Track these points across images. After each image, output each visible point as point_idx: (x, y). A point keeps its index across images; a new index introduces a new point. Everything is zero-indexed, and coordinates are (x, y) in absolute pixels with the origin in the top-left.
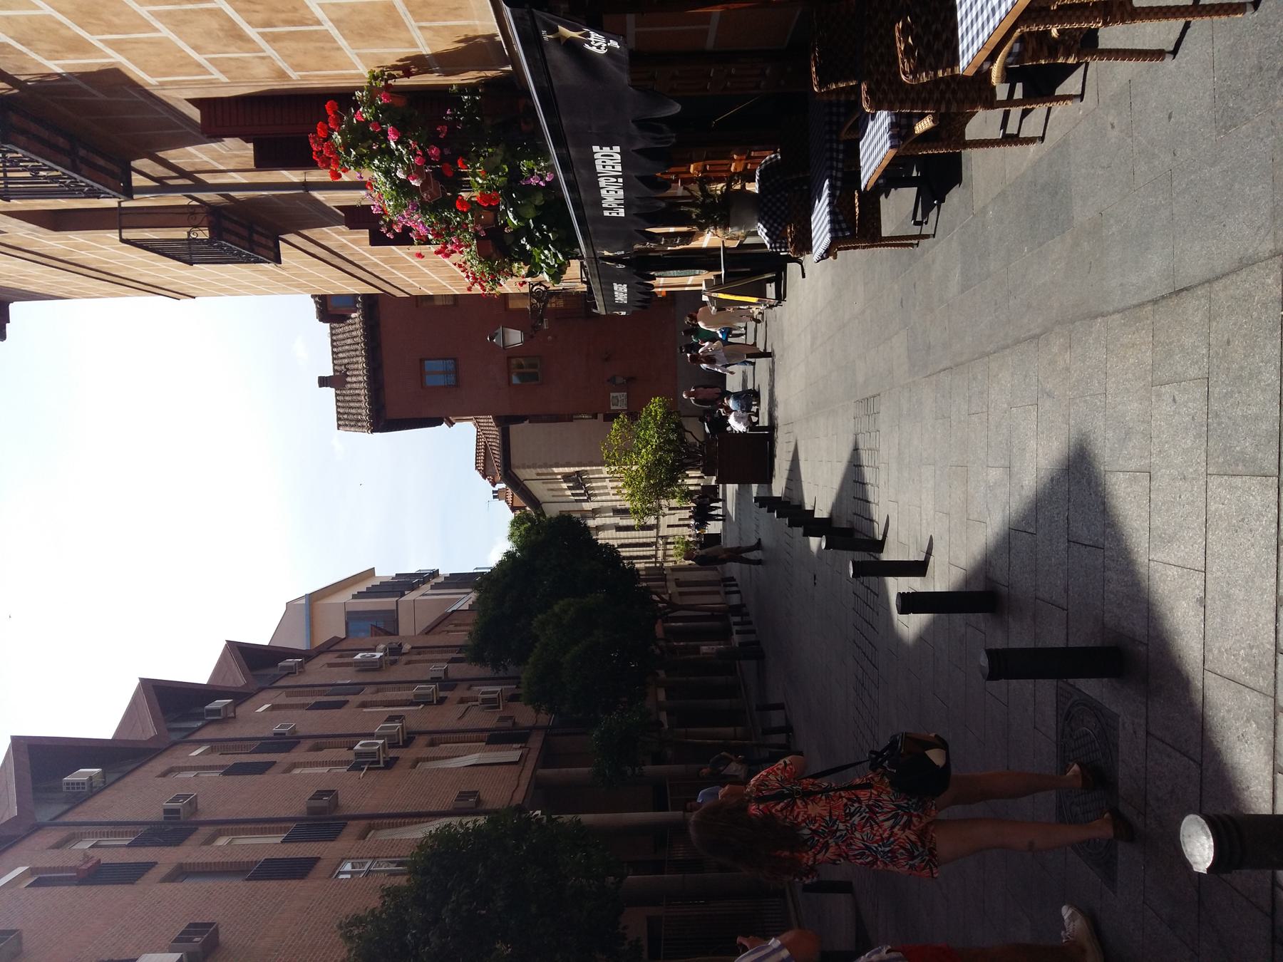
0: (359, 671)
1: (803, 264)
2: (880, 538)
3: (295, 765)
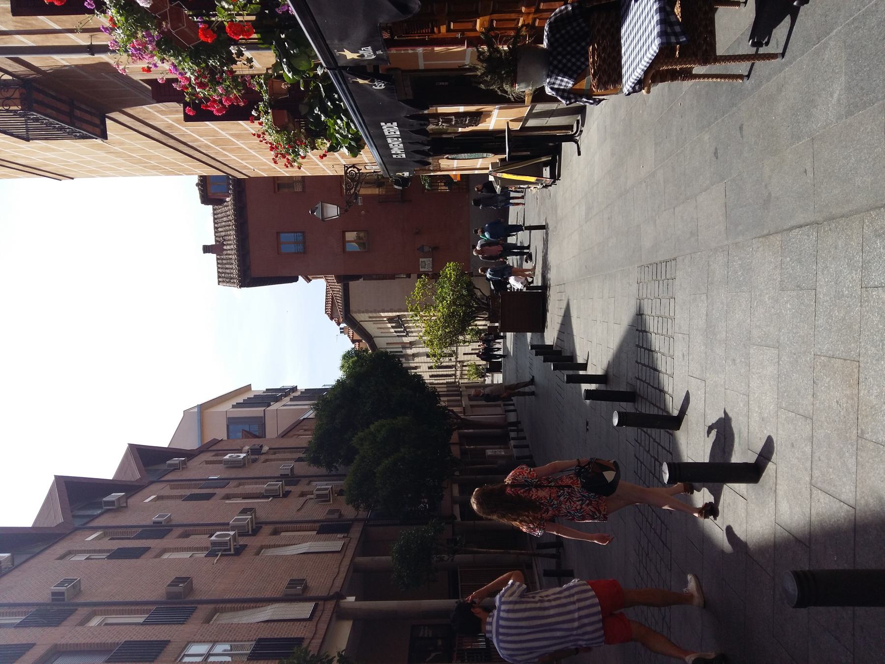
0: (227, 467)
1: (579, 143)
2: (675, 413)
3: (165, 551)
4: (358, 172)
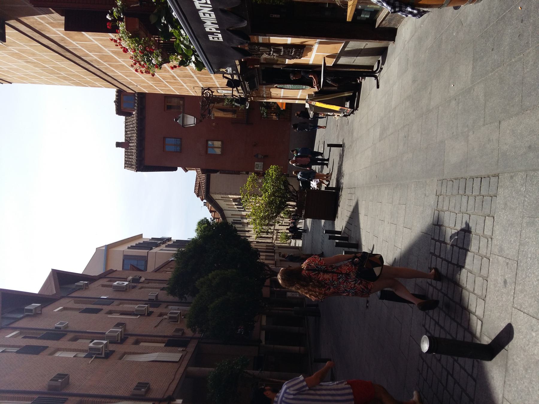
0: (115, 290)
3: (58, 350)
4: (211, 93)
